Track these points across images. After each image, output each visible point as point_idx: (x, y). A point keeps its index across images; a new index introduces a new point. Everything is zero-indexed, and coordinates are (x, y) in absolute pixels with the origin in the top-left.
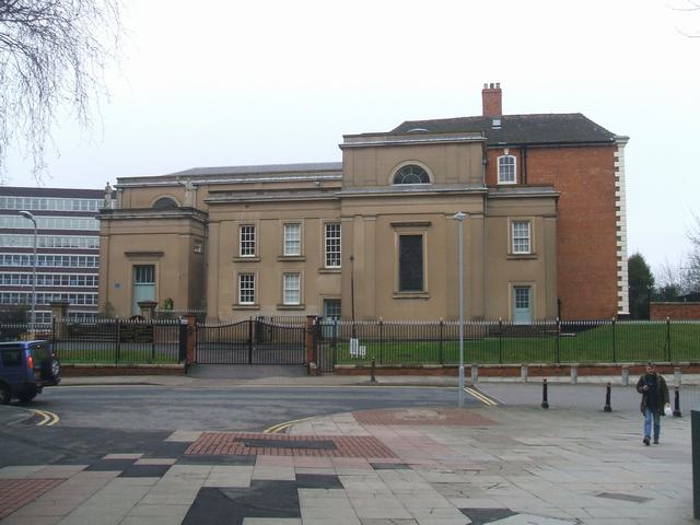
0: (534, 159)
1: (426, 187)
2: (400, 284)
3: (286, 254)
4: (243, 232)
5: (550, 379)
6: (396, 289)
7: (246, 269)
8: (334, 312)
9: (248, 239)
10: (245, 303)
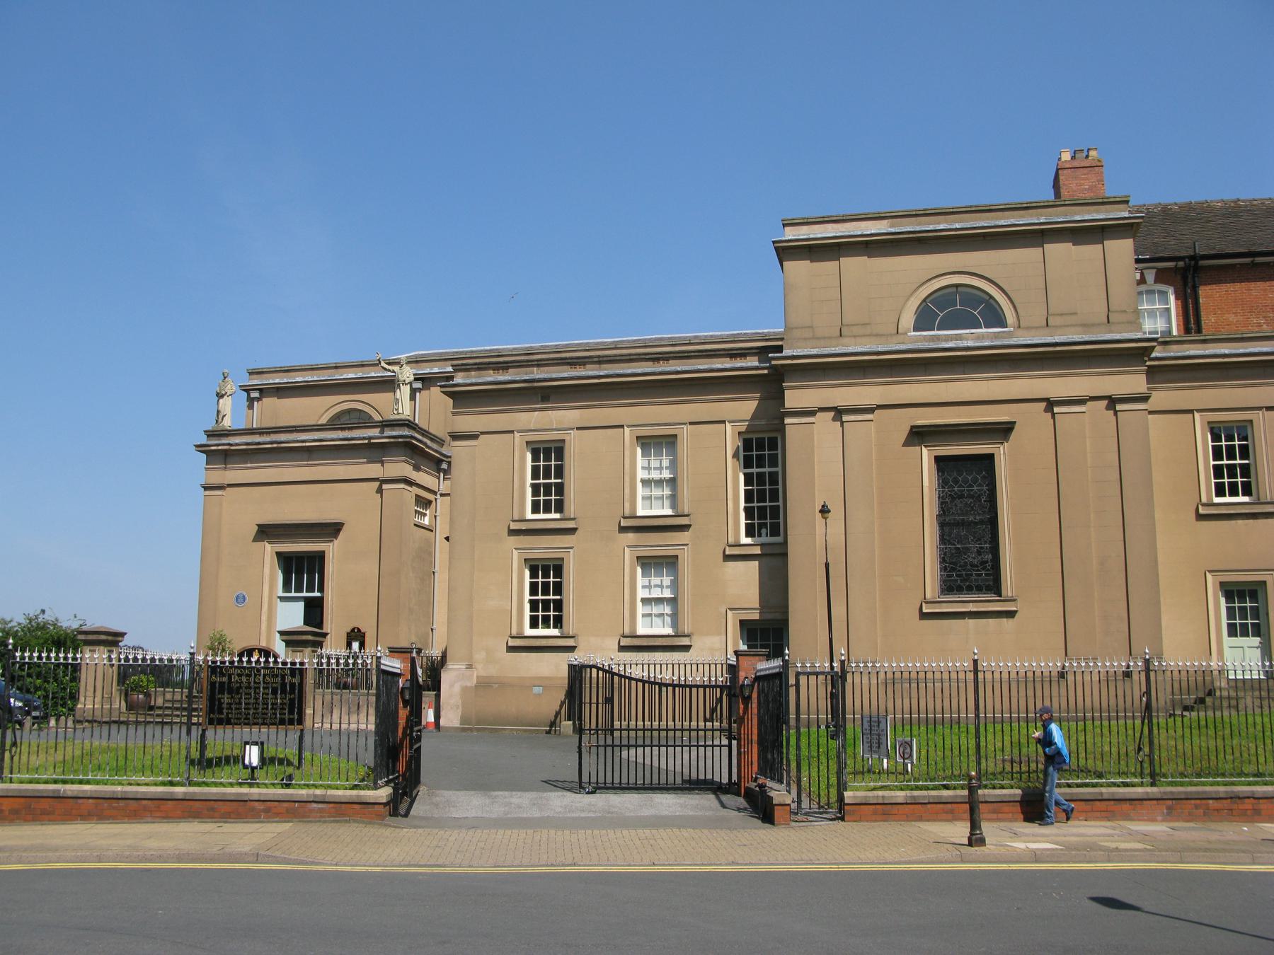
0: (1208, 295)
1: (996, 335)
2: (943, 581)
3: (640, 512)
4: (535, 458)
5: (658, 786)
6: (932, 589)
7: (544, 548)
8: (1232, 474)
9: (547, 476)
10: (541, 631)
